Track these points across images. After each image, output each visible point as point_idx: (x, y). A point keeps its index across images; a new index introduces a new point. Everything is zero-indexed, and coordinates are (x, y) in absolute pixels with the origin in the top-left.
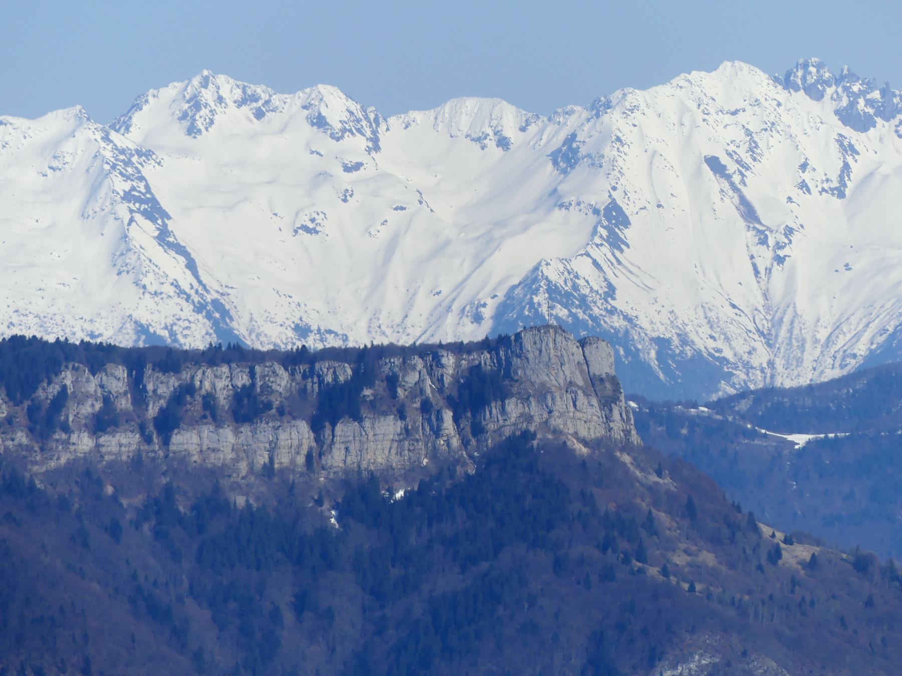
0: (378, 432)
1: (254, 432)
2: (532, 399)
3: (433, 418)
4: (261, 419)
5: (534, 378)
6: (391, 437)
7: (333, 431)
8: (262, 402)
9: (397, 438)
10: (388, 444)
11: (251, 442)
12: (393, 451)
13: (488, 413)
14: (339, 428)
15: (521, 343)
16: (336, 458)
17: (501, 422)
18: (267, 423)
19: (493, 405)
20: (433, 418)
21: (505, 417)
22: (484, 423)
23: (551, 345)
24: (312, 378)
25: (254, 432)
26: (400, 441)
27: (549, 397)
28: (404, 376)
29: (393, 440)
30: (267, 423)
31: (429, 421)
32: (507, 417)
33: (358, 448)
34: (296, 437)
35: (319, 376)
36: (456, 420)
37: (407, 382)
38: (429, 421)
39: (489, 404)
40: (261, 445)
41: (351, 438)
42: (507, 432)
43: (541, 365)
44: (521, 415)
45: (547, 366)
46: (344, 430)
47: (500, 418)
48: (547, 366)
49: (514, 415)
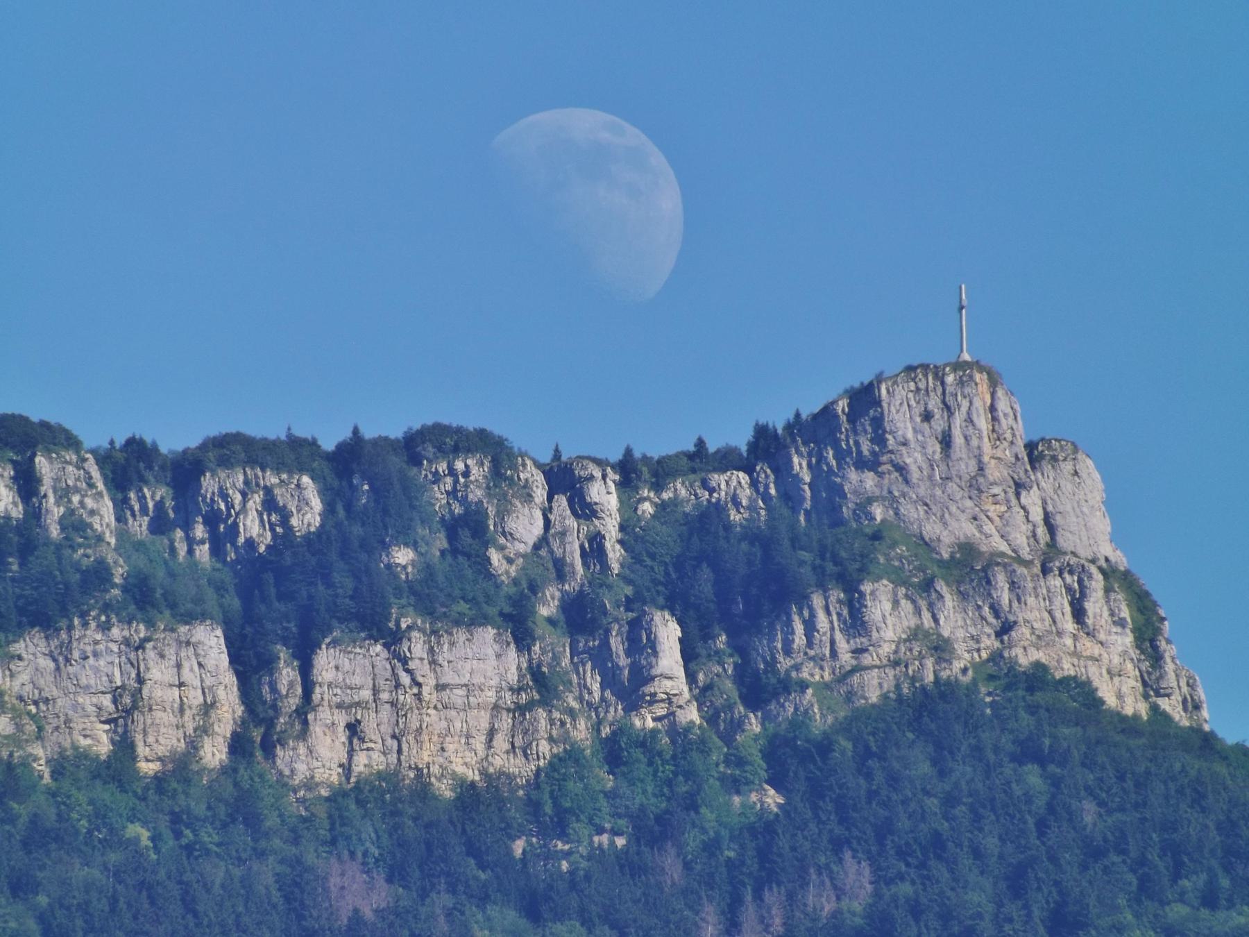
0: (449, 677)
1: (62, 657)
2: (941, 586)
3: (617, 644)
4: (83, 615)
5: (931, 529)
6: (490, 696)
7: (306, 670)
8: (77, 567)
9: (509, 699)
10: (483, 720)
11: (51, 691)
12: (501, 743)
13: (799, 628)
14: (326, 663)
15: (878, 422)
16: (318, 759)
17: (846, 658)
18: (105, 628)
19: (817, 601)
20: (617, 644)
21: (860, 642)
22: (784, 663)
23: (983, 423)
24: (187, 527)
25: (62, 657)
26: (520, 710)
27: (1001, 579)
28: (502, 515)
29: (496, 707)
30: (105, 628)
31: (601, 658)
32: (868, 647)
33: (386, 729)
34: (189, 683)
35: (212, 520)
36: (689, 655)
37: (510, 536)
38: (601, 658)
39: (803, 600)
40: (85, 700)
41: (366, 694)
42: (874, 687)
43: (952, 487)
44: (916, 634)
45: (975, 487)
46: (343, 667)
47: (843, 645)
48: (975, 487)
49: (889, 634)
